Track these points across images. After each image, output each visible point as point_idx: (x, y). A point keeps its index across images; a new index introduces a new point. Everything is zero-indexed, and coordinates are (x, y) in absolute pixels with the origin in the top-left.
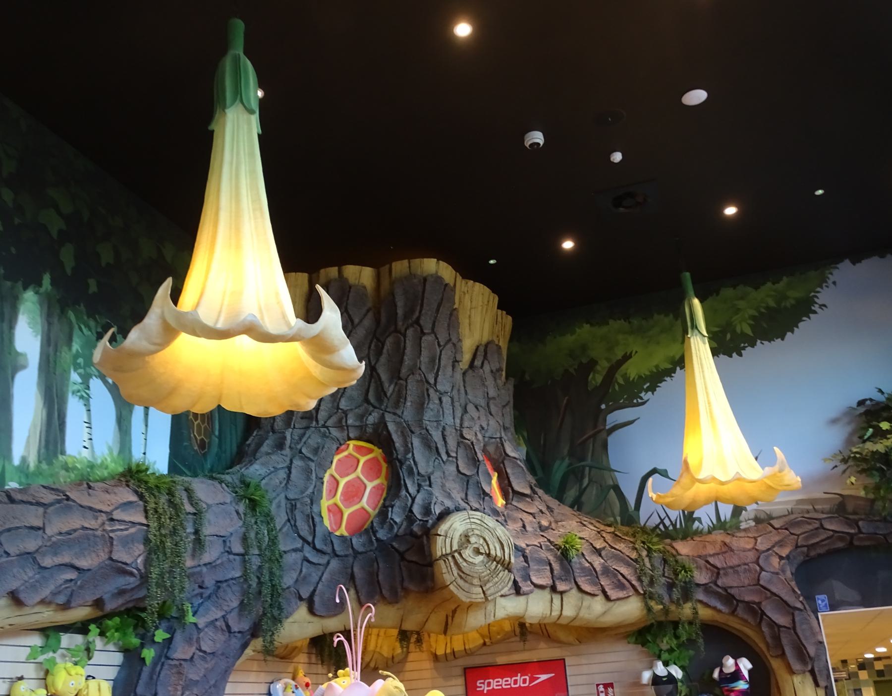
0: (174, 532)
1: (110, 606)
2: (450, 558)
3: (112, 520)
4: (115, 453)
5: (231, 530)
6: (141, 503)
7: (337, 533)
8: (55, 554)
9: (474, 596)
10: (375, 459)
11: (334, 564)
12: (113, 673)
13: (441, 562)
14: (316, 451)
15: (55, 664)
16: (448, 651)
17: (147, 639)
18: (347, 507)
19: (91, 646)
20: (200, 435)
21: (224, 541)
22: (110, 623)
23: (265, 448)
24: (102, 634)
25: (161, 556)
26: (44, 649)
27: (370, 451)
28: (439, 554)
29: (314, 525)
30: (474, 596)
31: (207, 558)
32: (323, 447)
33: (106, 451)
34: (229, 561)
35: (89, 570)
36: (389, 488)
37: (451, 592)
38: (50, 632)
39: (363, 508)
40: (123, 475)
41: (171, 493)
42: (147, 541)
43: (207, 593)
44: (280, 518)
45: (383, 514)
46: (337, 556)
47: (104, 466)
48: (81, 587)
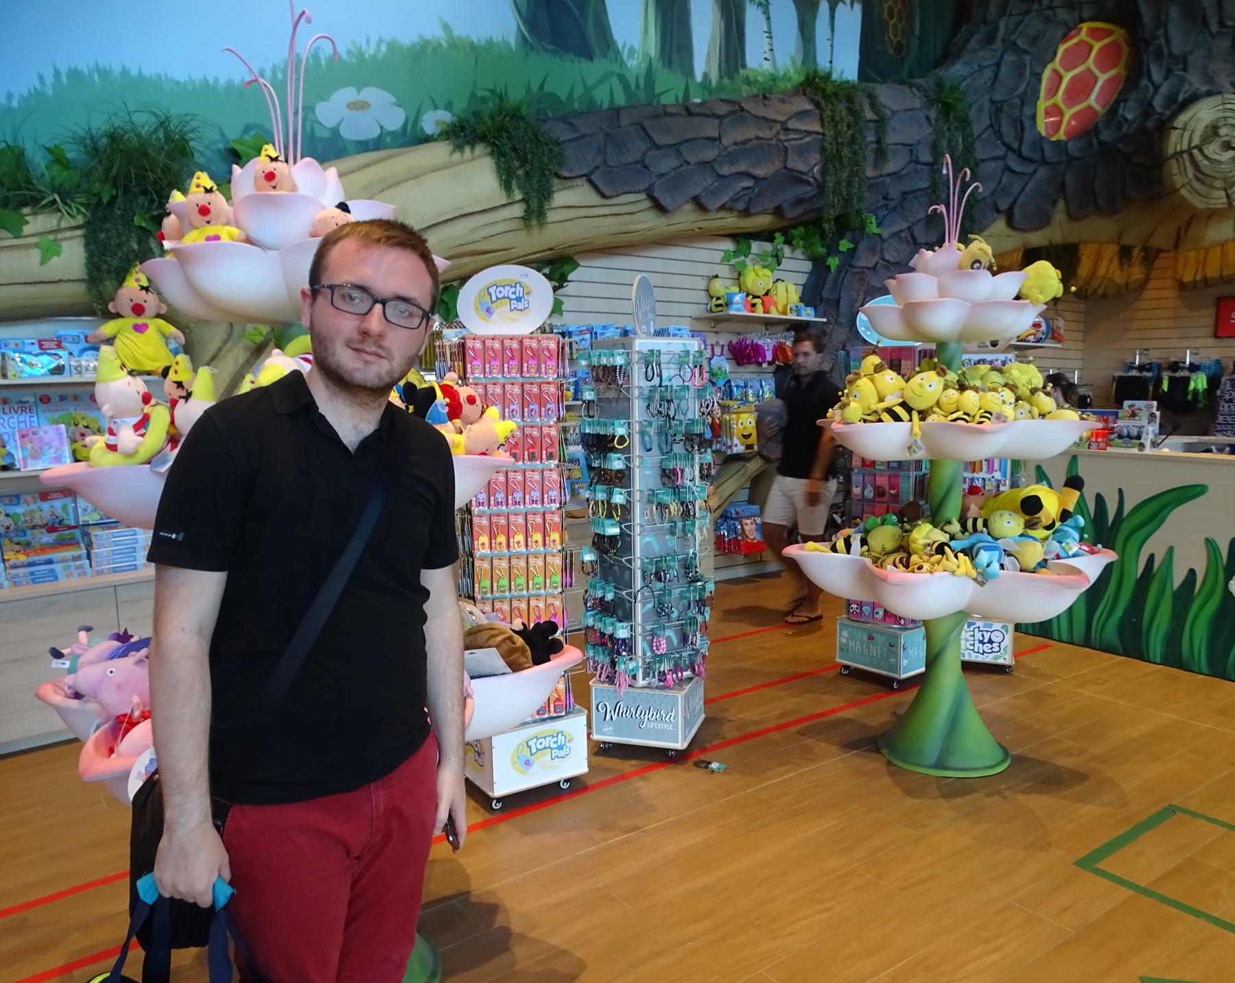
0: (853, 141)
1: (791, 214)
2: (1185, 156)
3: (787, 129)
4: (799, 63)
5: (918, 138)
6: (817, 111)
7: (1054, 139)
8: (732, 164)
9: (1213, 201)
10: (1114, 46)
11: (1043, 172)
12: (803, 279)
13: (1173, 161)
14: (1034, 41)
15: (745, 266)
16: (1199, 277)
17: (833, 250)
18: (1069, 107)
19: (780, 254)
20: (895, 35)
21: (911, 151)
22: (795, 232)
23: (973, 44)
24: (788, 242)
25: (837, 165)
26: (736, 253)
27: (1108, 33)
28: (1171, 151)
29: (1023, 130)
30: (1213, 201)
31: (890, 167)
32: (1044, 35)
33: (789, 62)
34: (916, 171)
35: (765, 179)
36: (1128, 78)
37: (1183, 197)
38: (741, 238)
39: (1090, 108)
40: (802, 84)
41: (850, 100)
42: (823, 150)
43: (893, 204)
44: (980, 124)
45: (1112, 112)
46: (1047, 163)
47: (786, 77)
48: (758, 195)
